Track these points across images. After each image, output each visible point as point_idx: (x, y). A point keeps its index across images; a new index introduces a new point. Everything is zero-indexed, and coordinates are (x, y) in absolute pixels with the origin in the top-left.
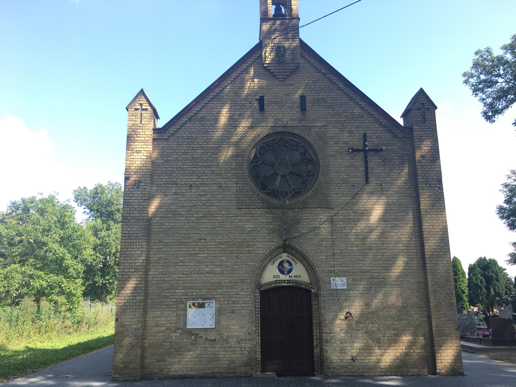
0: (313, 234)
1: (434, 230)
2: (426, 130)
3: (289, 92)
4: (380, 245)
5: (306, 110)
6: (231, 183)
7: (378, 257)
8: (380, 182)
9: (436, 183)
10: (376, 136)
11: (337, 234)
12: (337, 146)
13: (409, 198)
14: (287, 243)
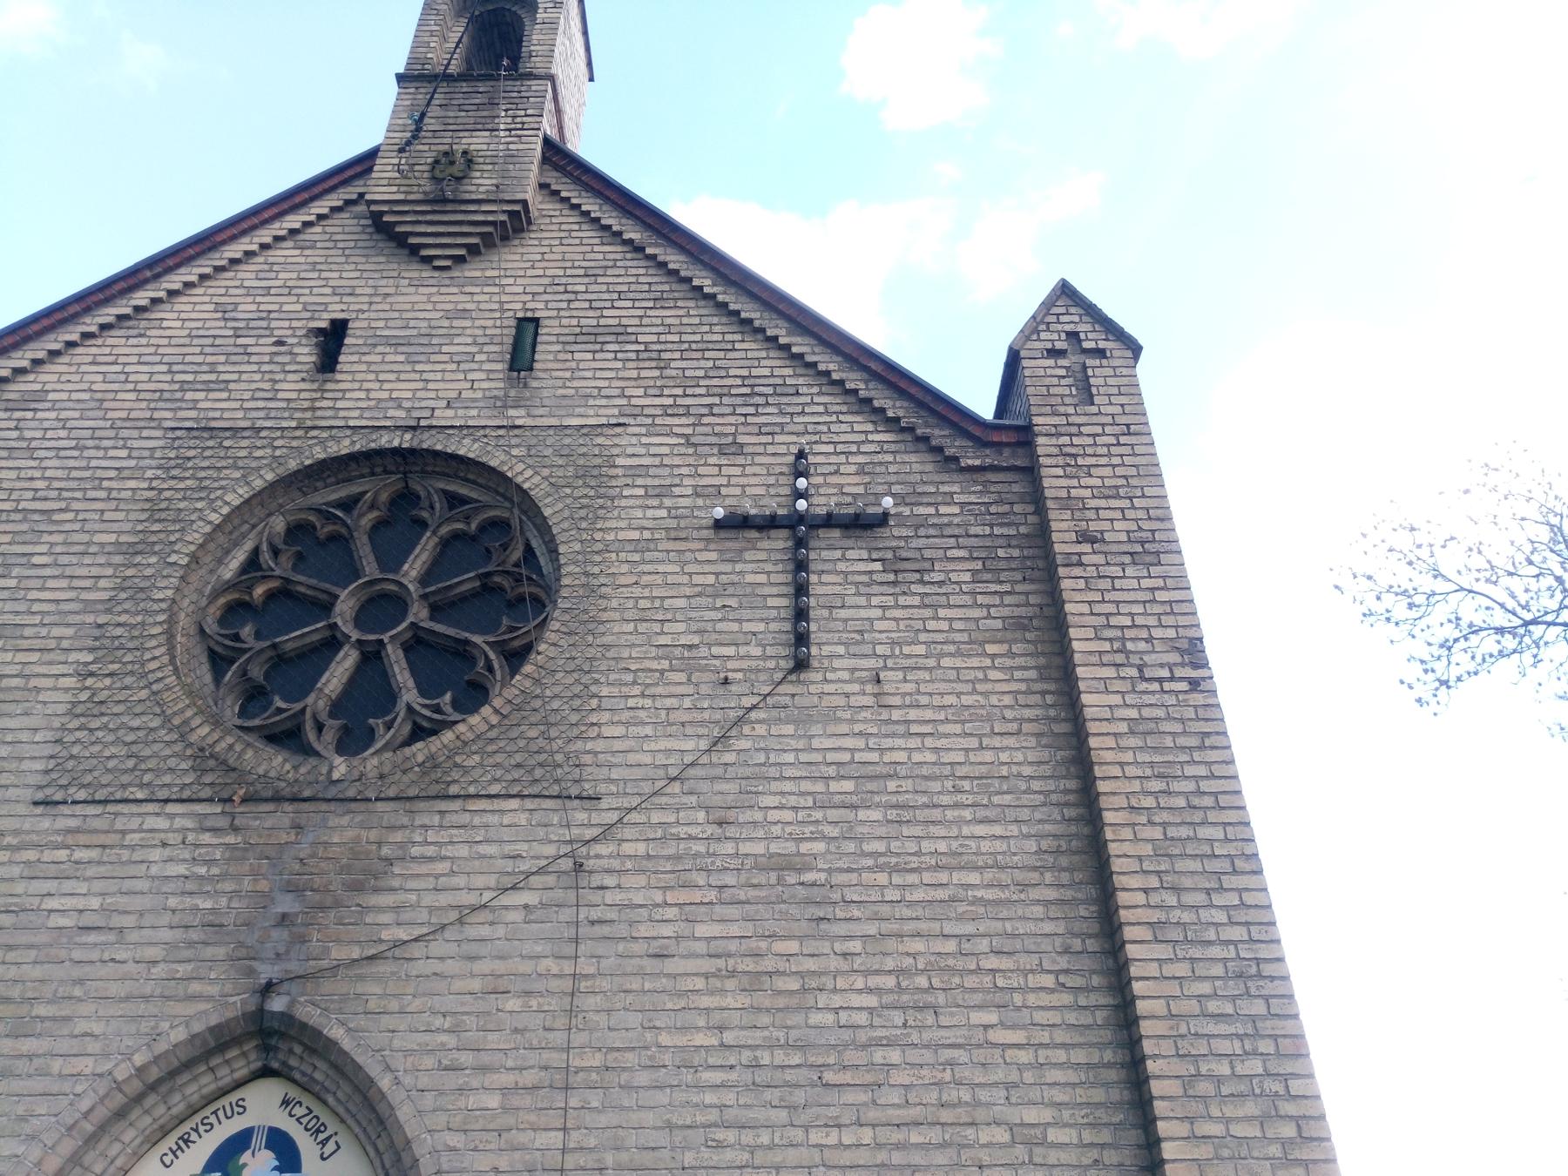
0: (452, 949)
1: (1187, 917)
2: (1099, 430)
3: (469, 306)
4: (861, 1018)
5: (531, 369)
6: (56, 669)
7: (850, 1097)
8: (871, 663)
9: (1174, 658)
10: (852, 461)
11: (601, 949)
12: (660, 507)
13: (1032, 742)
14: (277, 1004)
